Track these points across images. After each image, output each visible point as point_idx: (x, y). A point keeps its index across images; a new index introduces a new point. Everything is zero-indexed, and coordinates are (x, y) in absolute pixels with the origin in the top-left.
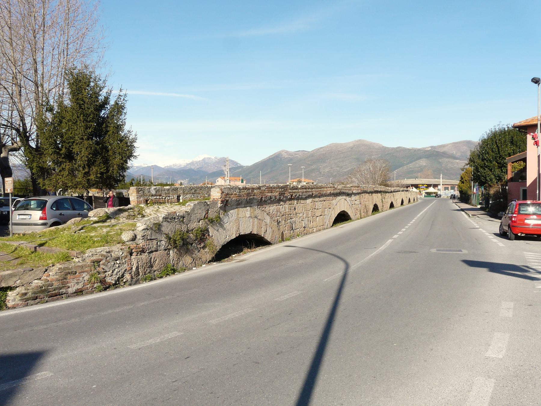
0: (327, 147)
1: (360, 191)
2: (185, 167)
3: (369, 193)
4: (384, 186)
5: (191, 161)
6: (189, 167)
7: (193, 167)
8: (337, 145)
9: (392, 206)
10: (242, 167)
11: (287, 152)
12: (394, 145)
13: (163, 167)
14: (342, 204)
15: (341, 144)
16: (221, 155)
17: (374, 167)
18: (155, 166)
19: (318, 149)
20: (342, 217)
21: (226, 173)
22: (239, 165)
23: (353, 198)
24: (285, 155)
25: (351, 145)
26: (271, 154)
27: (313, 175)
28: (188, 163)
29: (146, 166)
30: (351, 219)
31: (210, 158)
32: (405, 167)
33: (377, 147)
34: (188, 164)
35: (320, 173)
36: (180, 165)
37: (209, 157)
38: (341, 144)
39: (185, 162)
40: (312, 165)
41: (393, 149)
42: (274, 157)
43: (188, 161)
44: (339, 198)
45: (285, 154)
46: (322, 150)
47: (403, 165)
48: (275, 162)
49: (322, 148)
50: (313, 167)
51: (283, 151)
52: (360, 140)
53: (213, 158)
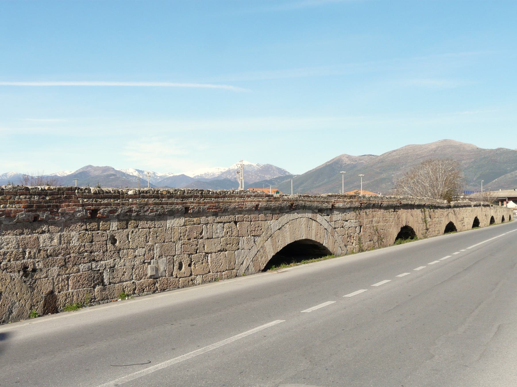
0: (402, 149)
1: (357, 204)
2: (219, 176)
3: (387, 208)
4: (450, 199)
5: (227, 169)
6: (224, 177)
7: (229, 177)
8: (414, 148)
9: (492, 221)
10: (291, 176)
11: (349, 157)
12: (494, 147)
13: (192, 176)
14: (412, 218)
15: (421, 146)
16: (264, 162)
17: (435, 171)
18: (183, 176)
19: (390, 153)
20: (406, 233)
21: (240, 183)
22: (287, 174)
23: (337, 216)
24: (346, 161)
25: (434, 147)
26: (329, 160)
27: (384, 186)
28: (223, 171)
29: (172, 175)
30: (456, 230)
31: (251, 166)
32: (509, 175)
33: (470, 149)
34: (223, 173)
35: (393, 183)
36: (214, 175)
37: (250, 163)
38: (420, 147)
39: (220, 171)
40: (382, 173)
41: (492, 151)
42: (332, 164)
43: (223, 169)
44: (286, 217)
45: (347, 159)
46: (394, 153)
47: (506, 172)
48: (332, 168)
49: (394, 151)
50: (384, 176)
51: (343, 156)
52: (445, 140)
53: (255, 165)
